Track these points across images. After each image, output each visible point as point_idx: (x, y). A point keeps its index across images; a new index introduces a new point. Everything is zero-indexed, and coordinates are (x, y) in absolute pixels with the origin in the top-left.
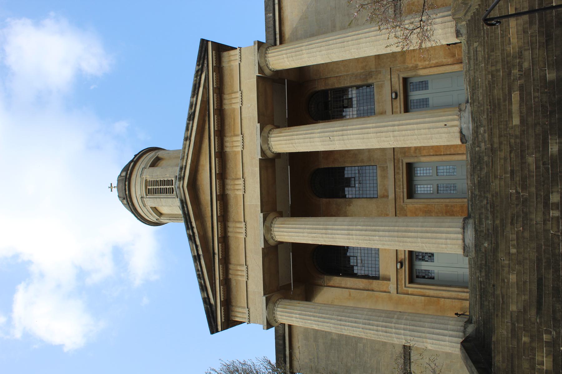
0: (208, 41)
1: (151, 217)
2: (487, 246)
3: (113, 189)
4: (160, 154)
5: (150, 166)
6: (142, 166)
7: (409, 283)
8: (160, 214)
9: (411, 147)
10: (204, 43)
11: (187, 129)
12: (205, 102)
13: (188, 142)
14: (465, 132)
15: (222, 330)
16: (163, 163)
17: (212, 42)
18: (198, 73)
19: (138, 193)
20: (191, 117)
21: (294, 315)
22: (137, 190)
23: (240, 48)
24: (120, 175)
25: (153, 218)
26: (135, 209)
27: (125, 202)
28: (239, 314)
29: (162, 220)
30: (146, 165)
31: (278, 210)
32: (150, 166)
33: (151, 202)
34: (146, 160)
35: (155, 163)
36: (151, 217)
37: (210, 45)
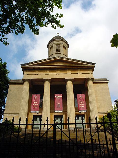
0: (95, 65)
1: (50, 45)
2: (35, 141)
3: (57, 34)
4: (67, 48)
5: (64, 46)
6: (64, 44)
7: (33, 115)
8: (51, 48)
9: (73, 85)
10: (94, 64)
11: (73, 59)
12: (79, 64)
13: (70, 59)
14: (67, 49)
15: (22, 68)
16: (64, 49)
17: (95, 66)
18: (87, 63)
19: (57, 43)
20: (76, 60)
21: (71, 103)
22: (58, 42)
23: (93, 74)
24: (61, 37)
25: (50, 46)
26: (52, 41)
27: (54, 38)
28: (26, 73)
29: (49, 49)
30: (64, 45)
31: (52, 82)
32: (64, 46)
33: (54, 46)
34: (65, 45)
35: (65, 47)
36: (50, 45)
37: (94, 66)
